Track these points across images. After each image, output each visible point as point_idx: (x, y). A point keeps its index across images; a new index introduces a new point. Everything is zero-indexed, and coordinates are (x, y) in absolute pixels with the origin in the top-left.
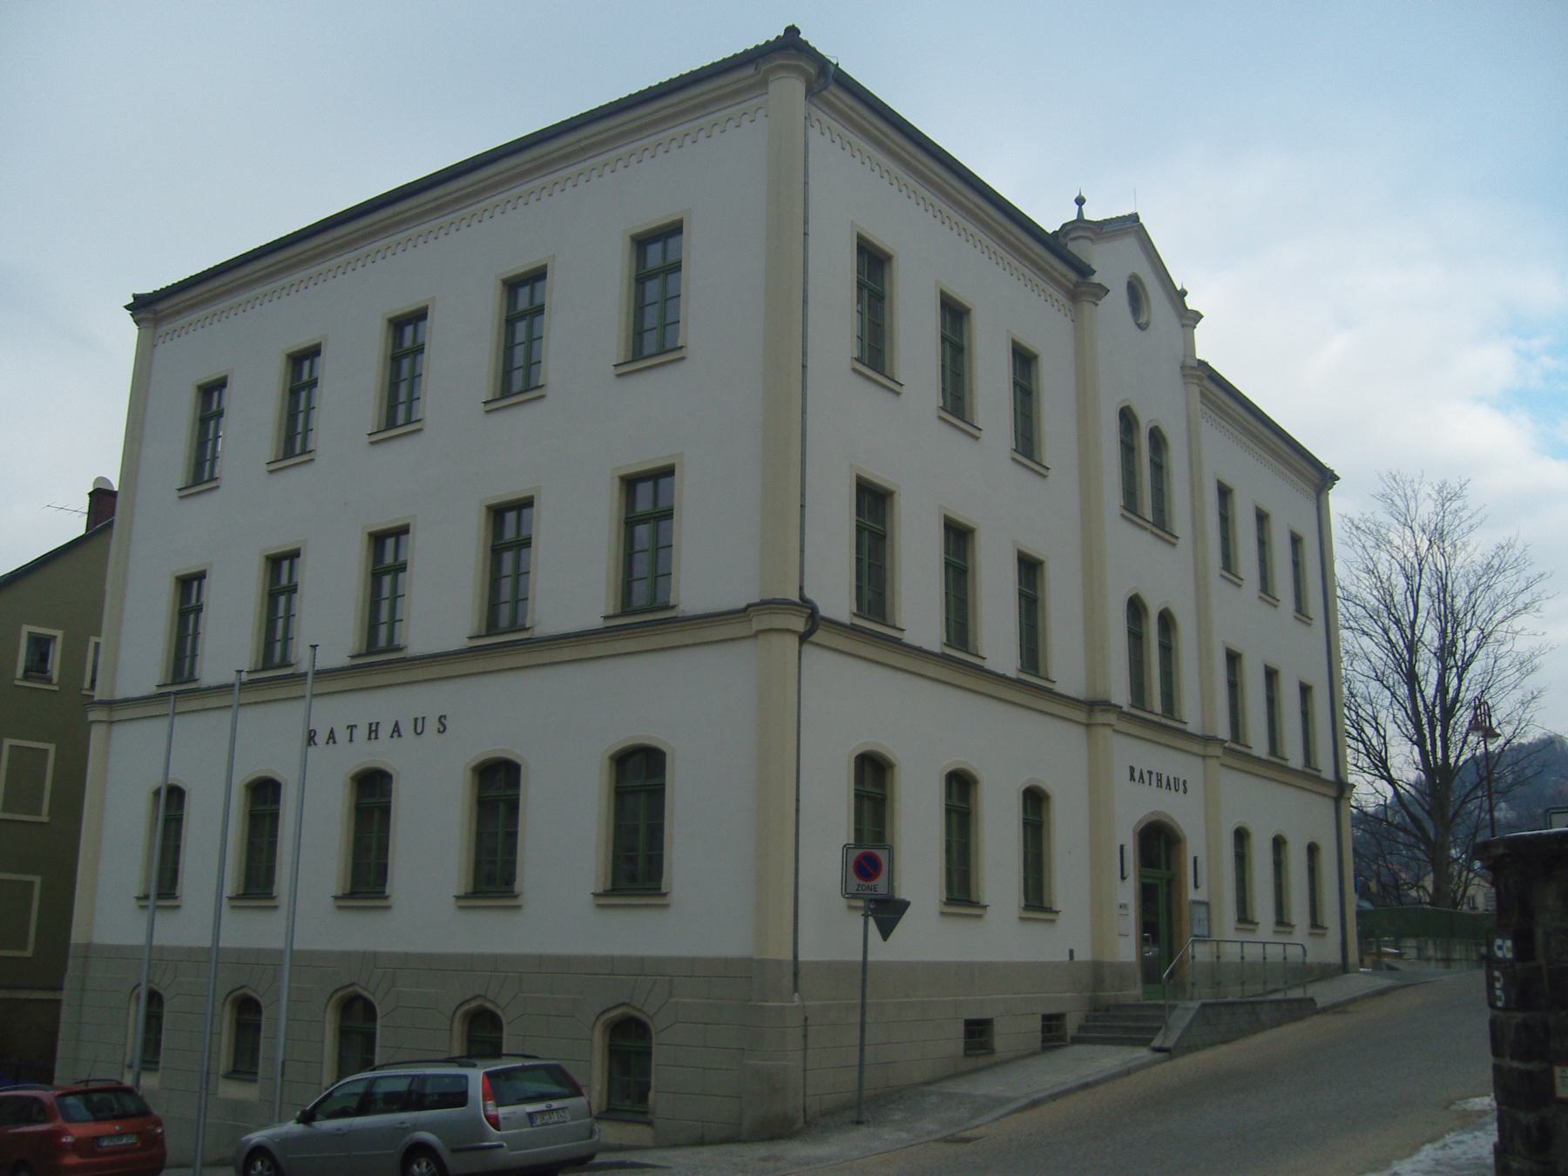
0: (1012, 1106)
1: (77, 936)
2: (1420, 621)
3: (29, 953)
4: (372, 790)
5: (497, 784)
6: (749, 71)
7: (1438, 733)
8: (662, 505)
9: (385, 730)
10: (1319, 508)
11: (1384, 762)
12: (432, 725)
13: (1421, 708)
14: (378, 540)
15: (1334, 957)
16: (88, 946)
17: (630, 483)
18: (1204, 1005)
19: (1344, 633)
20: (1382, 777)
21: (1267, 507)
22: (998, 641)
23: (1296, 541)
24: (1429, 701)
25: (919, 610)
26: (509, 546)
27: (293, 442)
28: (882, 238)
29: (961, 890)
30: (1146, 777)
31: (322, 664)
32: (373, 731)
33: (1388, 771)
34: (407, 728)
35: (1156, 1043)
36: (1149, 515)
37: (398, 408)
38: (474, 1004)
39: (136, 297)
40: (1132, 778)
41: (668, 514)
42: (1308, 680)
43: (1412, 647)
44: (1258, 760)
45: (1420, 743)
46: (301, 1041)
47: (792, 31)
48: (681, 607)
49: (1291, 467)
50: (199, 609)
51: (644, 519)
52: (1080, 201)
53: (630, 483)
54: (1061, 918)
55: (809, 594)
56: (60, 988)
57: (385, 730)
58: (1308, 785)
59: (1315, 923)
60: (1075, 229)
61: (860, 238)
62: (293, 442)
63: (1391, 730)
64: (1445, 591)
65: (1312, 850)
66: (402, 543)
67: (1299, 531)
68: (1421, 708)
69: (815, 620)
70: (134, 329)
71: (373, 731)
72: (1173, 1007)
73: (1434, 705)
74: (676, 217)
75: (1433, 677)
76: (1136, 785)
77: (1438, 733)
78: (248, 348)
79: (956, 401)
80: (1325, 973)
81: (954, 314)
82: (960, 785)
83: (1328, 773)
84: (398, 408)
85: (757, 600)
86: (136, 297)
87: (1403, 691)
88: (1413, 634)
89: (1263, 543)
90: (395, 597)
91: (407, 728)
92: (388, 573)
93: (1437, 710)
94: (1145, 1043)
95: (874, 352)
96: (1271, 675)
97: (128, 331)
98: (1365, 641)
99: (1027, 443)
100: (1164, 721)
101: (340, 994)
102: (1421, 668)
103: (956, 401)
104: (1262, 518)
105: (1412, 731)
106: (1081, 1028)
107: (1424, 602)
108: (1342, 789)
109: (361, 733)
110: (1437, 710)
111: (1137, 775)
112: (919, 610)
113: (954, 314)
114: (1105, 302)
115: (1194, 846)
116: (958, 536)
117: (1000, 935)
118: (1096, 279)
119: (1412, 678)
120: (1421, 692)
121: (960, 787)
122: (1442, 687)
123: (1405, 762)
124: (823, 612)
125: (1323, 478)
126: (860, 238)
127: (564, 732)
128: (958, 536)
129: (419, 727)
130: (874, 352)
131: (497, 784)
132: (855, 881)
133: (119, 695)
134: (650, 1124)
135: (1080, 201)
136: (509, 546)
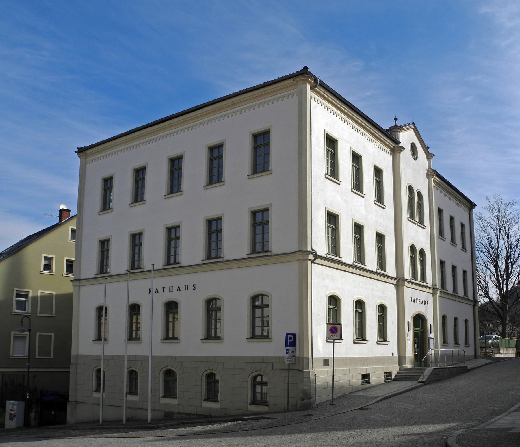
0: (378, 399)
1: (73, 352)
2: (500, 249)
3: (52, 357)
4: (172, 307)
5: (212, 306)
6: (291, 81)
7: (505, 283)
8: (265, 220)
9: (175, 289)
10: (470, 215)
11: (487, 292)
12: (191, 287)
13: (500, 276)
14: (169, 230)
15: (473, 353)
16: (77, 355)
17: (254, 213)
18: (434, 369)
19: (477, 252)
20: (486, 297)
21: (453, 215)
22: (371, 261)
23: (462, 225)
24: (502, 274)
25: (347, 253)
26: (214, 232)
27: (138, 196)
28: (334, 135)
29: (361, 334)
30: (416, 300)
31: (156, 267)
32: (171, 289)
33: (488, 295)
34: (182, 288)
35: (420, 380)
36: (417, 219)
37: (174, 186)
38: (209, 372)
39: (79, 149)
40: (411, 301)
41: (267, 223)
42: (466, 269)
43: (497, 256)
44: (450, 294)
45: (499, 287)
46: (151, 382)
47: (306, 68)
48: (273, 252)
49: (459, 201)
50: (108, 250)
51: (259, 224)
52: (396, 119)
53: (254, 213)
54: (389, 344)
55: (314, 248)
56: (69, 368)
57: (175, 289)
58: (465, 301)
59: (467, 343)
60: (394, 128)
61: (327, 134)
62: (138, 196)
63: (490, 284)
64: (508, 239)
65: (466, 321)
66: (177, 231)
67: (463, 222)
68: (500, 276)
69: (316, 256)
70: (79, 160)
71: (171, 289)
72: (425, 369)
73: (504, 274)
74: (267, 128)
75: (504, 265)
76: (412, 303)
77: (505, 283)
78: (120, 166)
79: (358, 186)
80: (468, 359)
81: (357, 158)
82: (360, 304)
83: (471, 298)
84: (174, 186)
85: (298, 250)
86: (79, 149)
87: (493, 269)
88: (497, 252)
89: (452, 227)
90: (176, 247)
91: (182, 288)
92: (173, 240)
93: (505, 276)
94: (417, 380)
95: (333, 171)
96: (454, 268)
97: (77, 160)
98: (482, 254)
99: (380, 199)
100: (421, 283)
101: (164, 369)
102: (500, 263)
103: (358, 186)
104: (452, 219)
105: (496, 281)
106: (395, 376)
107: (501, 242)
108: (475, 302)
109: (167, 290)
110: (505, 276)
111: (413, 300)
112: (347, 253)
113: (357, 158)
114: (403, 152)
115: (430, 321)
116: (358, 228)
117: (371, 348)
118: (401, 145)
119: (496, 266)
120: (500, 271)
121: (360, 304)
122: (507, 269)
123: (494, 293)
124: (318, 254)
125: (471, 205)
126: (327, 134)
127: (233, 288)
128: (358, 228)
129: (186, 288)
130: (333, 171)
131: (212, 306)
132: (330, 334)
133: (82, 278)
134: (267, 406)
135: (396, 119)
136: (214, 232)
